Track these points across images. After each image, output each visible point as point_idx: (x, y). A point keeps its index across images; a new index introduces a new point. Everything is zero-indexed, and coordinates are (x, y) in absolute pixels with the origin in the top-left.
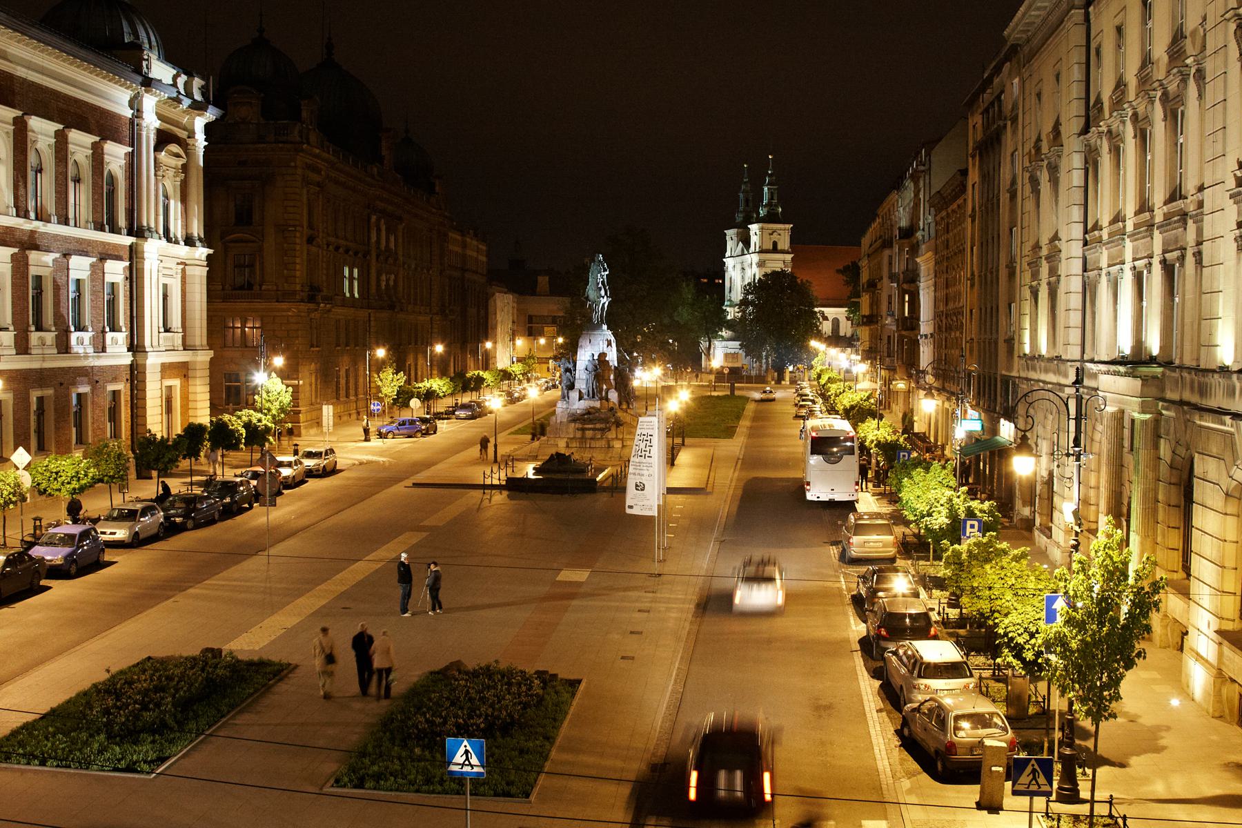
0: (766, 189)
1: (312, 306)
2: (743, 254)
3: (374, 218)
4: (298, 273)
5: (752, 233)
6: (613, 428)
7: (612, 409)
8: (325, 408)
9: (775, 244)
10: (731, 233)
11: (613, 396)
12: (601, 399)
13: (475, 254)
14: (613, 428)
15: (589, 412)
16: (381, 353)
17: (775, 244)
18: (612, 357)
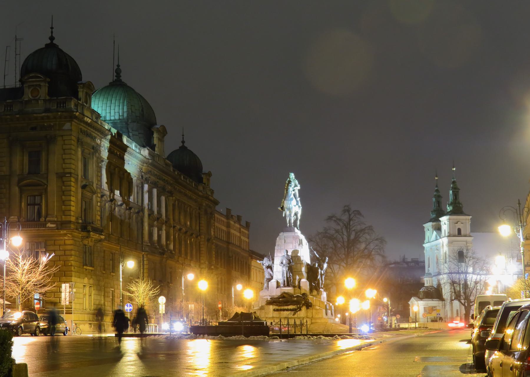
0: (451, 192)
1: (84, 234)
2: (437, 240)
3: (146, 187)
4: (73, 208)
5: (442, 223)
6: (304, 308)
7: (304, 294)
8: (63, 285)
9: (459, 230)
10: (428, 226)
11: (305, 283)
12: (294, 287)
13: (238, 234)
14: (304, 308)
15: (284, 296)
16: (130, 264)
17: (459, 230)
18: (305, 254)
